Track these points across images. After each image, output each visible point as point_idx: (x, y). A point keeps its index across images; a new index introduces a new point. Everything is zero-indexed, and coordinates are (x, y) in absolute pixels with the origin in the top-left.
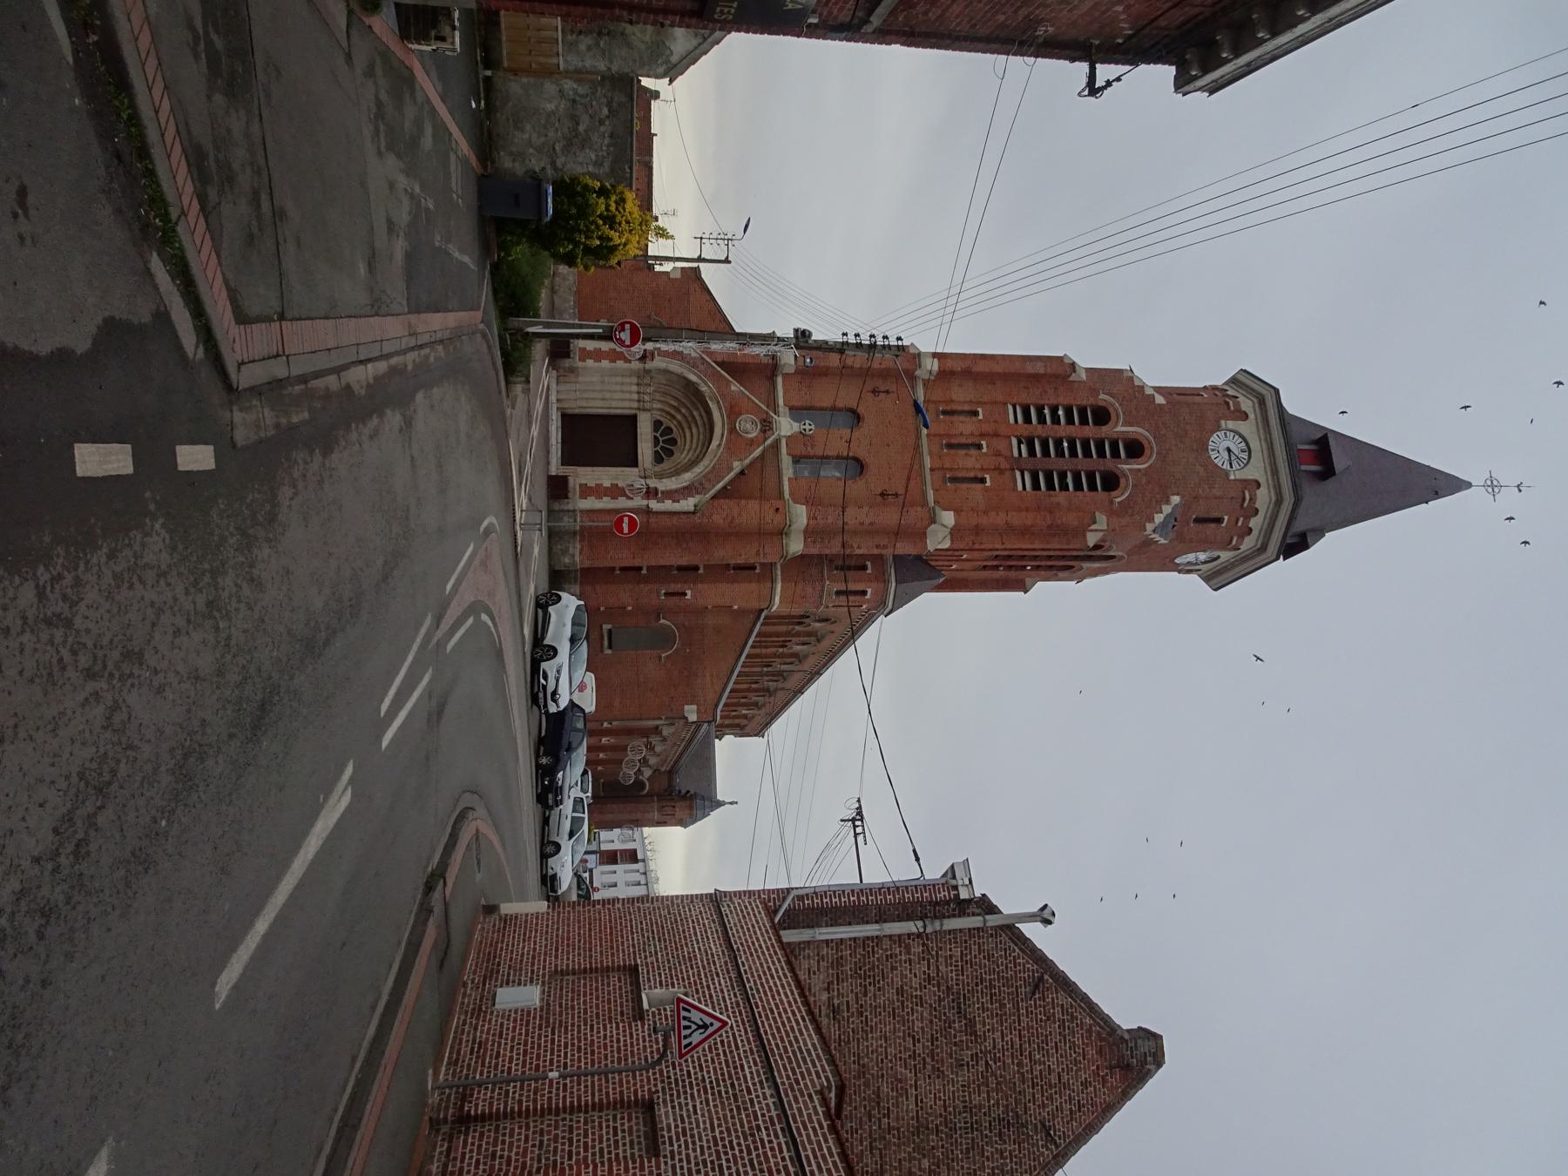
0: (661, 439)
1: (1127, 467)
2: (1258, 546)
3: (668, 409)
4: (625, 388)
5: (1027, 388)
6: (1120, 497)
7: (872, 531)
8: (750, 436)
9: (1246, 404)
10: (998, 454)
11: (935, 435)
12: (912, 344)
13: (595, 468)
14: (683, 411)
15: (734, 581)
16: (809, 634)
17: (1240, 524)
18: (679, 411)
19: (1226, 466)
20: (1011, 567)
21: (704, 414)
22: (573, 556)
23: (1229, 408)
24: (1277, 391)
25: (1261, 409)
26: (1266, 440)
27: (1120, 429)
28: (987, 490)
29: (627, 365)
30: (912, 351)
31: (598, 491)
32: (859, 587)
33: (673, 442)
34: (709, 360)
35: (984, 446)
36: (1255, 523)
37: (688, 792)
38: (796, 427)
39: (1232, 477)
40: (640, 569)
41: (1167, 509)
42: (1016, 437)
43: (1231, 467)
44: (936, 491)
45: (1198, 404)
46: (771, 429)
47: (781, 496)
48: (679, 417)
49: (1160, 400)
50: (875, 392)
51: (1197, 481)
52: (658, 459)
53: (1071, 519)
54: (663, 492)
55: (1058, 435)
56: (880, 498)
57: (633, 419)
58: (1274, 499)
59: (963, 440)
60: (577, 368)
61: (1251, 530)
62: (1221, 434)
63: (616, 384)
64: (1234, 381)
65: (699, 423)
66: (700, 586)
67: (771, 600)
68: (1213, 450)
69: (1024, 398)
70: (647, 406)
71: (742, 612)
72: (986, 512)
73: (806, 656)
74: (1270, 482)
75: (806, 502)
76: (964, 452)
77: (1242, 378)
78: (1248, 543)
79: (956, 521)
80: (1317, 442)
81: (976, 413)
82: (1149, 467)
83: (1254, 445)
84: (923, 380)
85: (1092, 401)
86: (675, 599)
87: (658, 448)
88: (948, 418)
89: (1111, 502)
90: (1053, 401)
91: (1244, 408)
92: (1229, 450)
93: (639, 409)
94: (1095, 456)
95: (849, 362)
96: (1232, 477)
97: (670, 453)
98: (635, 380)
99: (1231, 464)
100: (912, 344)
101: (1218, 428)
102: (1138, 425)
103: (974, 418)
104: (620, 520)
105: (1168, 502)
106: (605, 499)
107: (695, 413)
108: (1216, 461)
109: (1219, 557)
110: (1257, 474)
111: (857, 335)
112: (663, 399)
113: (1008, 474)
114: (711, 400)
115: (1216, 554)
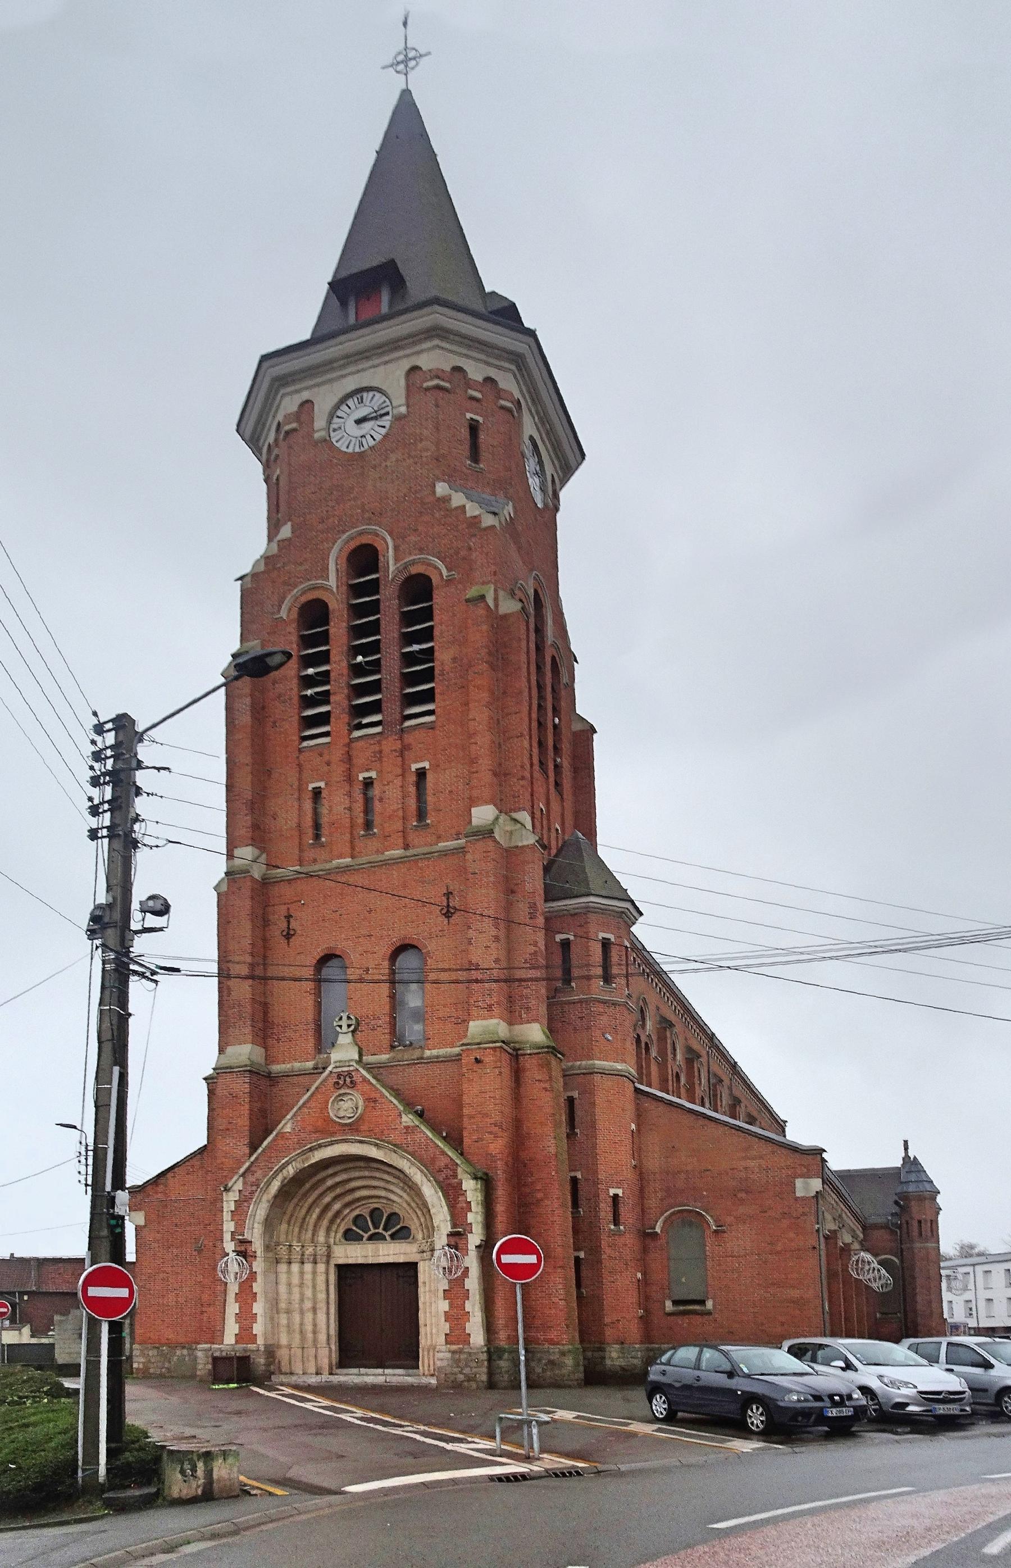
0: (373, 1231)
1: (391, 566)
2: (513, 367)
3: (325, 1223)
4: (295, 1280)
5: (275, 722)
6: (440, 570)
7: (507, 922)
8: (361, 1103)
9: (289, 405)
10: (379, 755)
11: (353, 848)
12: (215, 888)
13: (421, 1322)
14: (327, 1199)
15: (593, 1125)
16: (662, 1039)
17: (478, 395)
18: (327, 1207)
19: (386, 421)
20: (555, 748)
21: (330, 1171)
22: (563, 1354)
23: (294, 430)
24: (264, 358)
25: (294, 381)
26: (343, 366)
27: (332, 582)
28: (435, 766)
29: (259, 1278)
30: (224, 888)
31: (457, 1317)
32: (597, 949)
33: (375, 1213)
34: (247, 1164)
35: (367, 775)
36: (476, 372)
37: (896, 1203)
38: (345, 1039)
39: (403, 410)
40: (577, 1260)
41: (458, 499)
42: (350, 732)
43: (387, 414)
44: (439, 838)
45: (290, 474)
46: (349, 1074)
47: (457, 1059)
48: (337, 1206)
49: (286, 532)
50: (288, 936)
51: (411, 461)
52: (402, 1234)
53: (479, 636)
54: (454, 1225)
55: (345, 672)
56: (455, 917)
57: (344, 1271)
58: (436, 342)
59: (359, 806)
60: (266, 1346)
61: (489, 380)
62: (335, 437)
63: (290, 1293)
64: (254, 442)
65: (344, 1176)
66: (602, 1176)
67: (619, 1074)
68: (361, 444)
69: (291, 725)
70: (322, 1250)
71: (640, 1116)
72: (473, 761)
73: (689, 1050)
74: (408, 351)
75: (463, 1022)
76: (377, 803)
77: (249, 429)
78: (507, 382)
79: (487, 803)
80: (344, 304)
81: (317, 793)
82: (391, 534)
83: (350, 384)
84: (267, 869)
85: (292, 628)
86: (623, 1210)
87: (387, 1234)
88: (325, 831)
89: (449, 581)
90: (294, 683)
91: (294, 408)
92: (359, 422)
93: (328, 1262)
94: (378, 656)
95: (245, 971)
96: (403, 410)
97: (393, 1217)
98: (283, 1267)
99: (382, 416)
100: (215, 888)
101: (327, 442)
102: (325, 559)
103: (323, 795)
104: (512, 1270)
105: (446, 499)
106: (468, 1306)
107: (330, 1183)
108: (378, 438)
109: (531, 438)
110: (398, 372)
111: (94, 811)
112: (311, 1227)
113: (409, 739)
114: (307, 1159)
115: (527, 449)
